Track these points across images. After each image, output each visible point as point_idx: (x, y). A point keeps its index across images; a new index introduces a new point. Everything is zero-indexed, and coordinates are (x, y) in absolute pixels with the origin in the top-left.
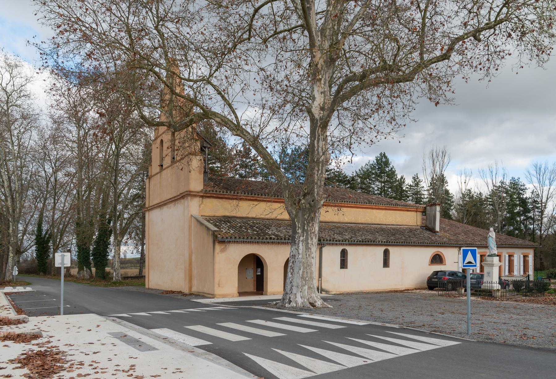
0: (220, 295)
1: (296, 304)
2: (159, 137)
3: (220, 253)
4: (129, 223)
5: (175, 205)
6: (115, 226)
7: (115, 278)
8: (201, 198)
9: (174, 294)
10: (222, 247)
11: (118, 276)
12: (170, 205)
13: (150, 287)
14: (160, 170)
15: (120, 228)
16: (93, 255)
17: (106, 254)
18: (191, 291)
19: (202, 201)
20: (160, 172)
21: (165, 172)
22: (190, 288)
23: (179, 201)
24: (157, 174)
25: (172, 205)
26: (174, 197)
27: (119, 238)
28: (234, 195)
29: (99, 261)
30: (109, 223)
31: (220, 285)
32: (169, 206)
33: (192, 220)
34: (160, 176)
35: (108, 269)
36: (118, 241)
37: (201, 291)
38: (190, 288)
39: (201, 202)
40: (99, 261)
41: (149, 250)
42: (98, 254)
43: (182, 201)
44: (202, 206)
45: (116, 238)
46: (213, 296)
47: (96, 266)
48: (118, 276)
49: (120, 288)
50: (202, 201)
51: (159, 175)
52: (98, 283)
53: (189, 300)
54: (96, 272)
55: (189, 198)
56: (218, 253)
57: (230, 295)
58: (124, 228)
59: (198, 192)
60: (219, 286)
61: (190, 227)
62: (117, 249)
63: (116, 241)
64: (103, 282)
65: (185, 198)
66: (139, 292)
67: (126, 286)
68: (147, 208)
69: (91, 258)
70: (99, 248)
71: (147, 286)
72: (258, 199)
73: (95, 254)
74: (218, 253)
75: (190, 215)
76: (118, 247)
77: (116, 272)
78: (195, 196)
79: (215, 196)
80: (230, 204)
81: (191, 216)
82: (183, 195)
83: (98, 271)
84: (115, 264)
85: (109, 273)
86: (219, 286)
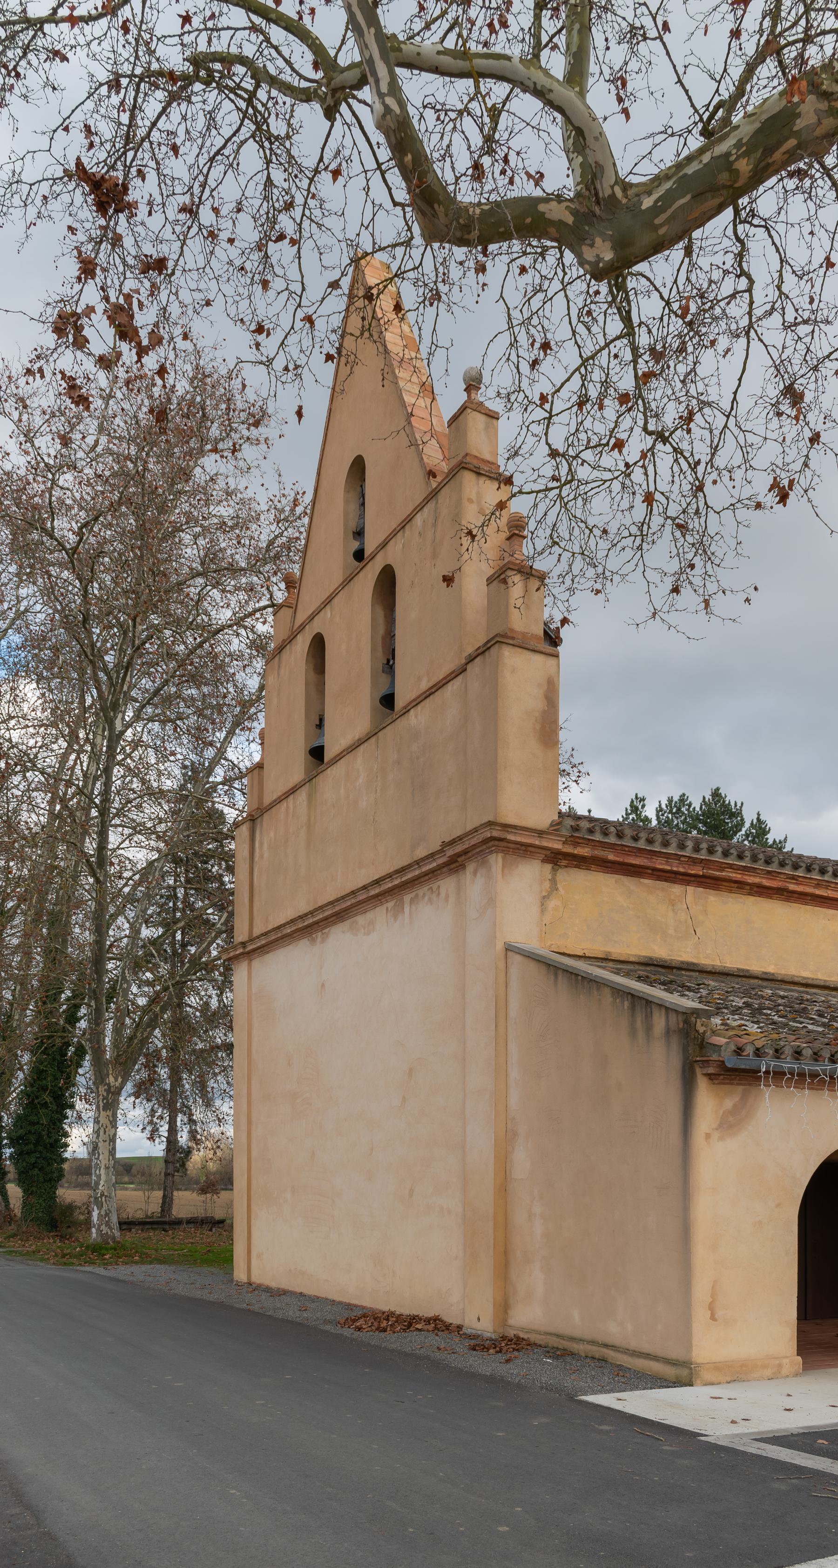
0: (718, 1367)
1: (786, 1357)
2: (302, 628)
3: (716, 1135)
4: (149, 1025)
5: (399, 909)
6: (96, 1034)
7: (99, 1231)
8: (549, 867)
9: (412, 1336)
10: (729, 1103)
11: (108, 1224)
12: (370, 915)
13: (256, 1278)
14: (307, 771)
15: (115, 1044)
16: (13, 1142)
17: (57, 1141)
18: (504, 1323)
19: (553, 882)
20: (310, 779)
21: (333, 775)
22: (504, 1307)
23: (422, 891)
24: (293, 791)
25: (379, 915)
26: (402, 870)
27: (111, 1079)
28: (694, 861)
29: (34, 1166)
30: (72, 1019)
31: (720, 1313)
32: (361, 920)
33: (514, 971)
34: (310, 798)
35: (67, 1194)
36: (108, 1091)
37: (577, 1333)
38: (504, 1307)
39: (547, 885)
40: (34, 1166)
41: (249, 1123)
42: (32, 1138)
43: (447, 884)
44: (552, 903)
45: (100, 1077)
46: (684, 1372)
47: (23, 1179)
48: (108, 1224)
49: (122, 1271)
50: (553, 882)
51: (302, 796)
52: (31, 1245)
53: (571, 1398)
54: (25, 1204)
55: (496, 861)
56: (708, 1136)
57: (765, 1367)
58: (131, 1039)
59: (540, 833)
60: (713, 1318)
61: (501, 1005)
62: (103, 1120)
63: (102, 1089)
64: (52, 1243)
65: (471, 867)
66: (249, 1310)
67: (142, 1262)
68: (243, 944)
69: (8, 1152)
70: (34, 1118)
71: (240, 1274)
72: (792, 887)
73: (20, 1138)
74: (708, 1136)
75: (500, 946)
76: (110, 1113)
77: (100, 1207)
78: (525, 850)
79: (611, 857)
80: (672, 903)
81: (509, 949)
82: (459, 848)
83: (33, 1200)
84: (99, 1177)
85: (70, 1208)
86: (713, 1318)
